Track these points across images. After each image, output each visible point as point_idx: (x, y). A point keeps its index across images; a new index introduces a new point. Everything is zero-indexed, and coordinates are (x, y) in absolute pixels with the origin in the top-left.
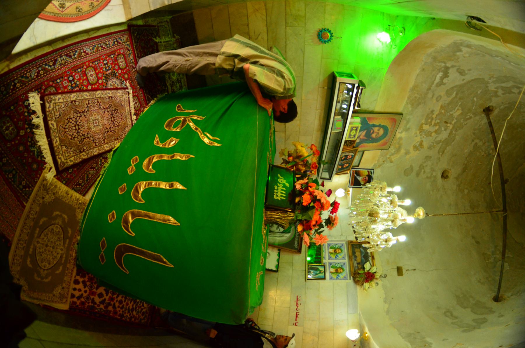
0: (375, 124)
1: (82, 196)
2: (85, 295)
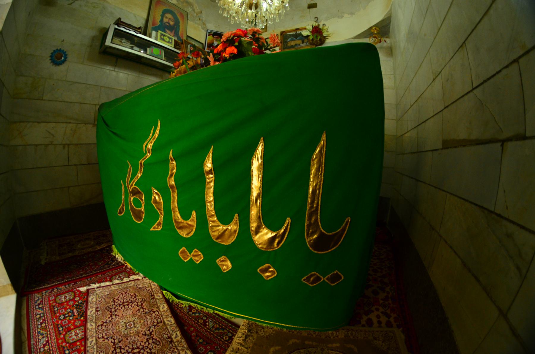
0: (159, 20)
1: (240, 330)
2: (381, 309)
